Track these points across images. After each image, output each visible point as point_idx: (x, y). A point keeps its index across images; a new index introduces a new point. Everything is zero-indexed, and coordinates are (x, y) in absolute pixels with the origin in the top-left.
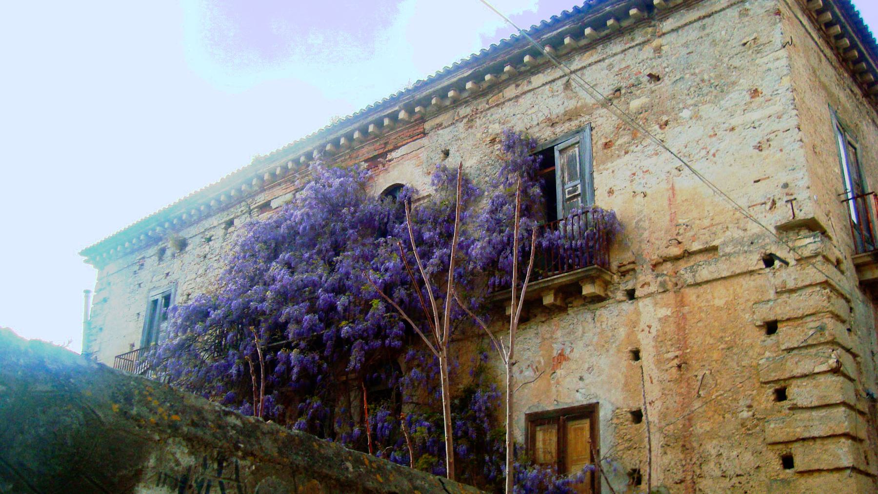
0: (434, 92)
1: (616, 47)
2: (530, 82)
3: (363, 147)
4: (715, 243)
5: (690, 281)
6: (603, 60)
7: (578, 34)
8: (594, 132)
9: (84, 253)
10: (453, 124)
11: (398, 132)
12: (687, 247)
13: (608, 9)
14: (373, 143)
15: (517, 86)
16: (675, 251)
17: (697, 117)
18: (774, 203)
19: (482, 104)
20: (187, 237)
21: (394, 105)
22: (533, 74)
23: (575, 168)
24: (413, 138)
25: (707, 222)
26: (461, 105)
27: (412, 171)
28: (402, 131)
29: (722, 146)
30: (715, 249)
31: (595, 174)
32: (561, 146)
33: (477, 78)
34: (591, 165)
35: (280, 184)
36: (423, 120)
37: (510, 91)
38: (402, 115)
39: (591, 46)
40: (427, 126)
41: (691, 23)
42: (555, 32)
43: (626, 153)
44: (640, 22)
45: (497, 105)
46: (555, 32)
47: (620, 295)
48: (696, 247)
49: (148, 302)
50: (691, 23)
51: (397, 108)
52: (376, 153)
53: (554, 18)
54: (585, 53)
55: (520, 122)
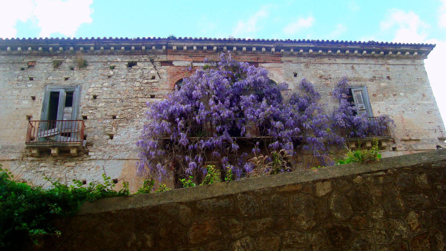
0: (294, 47)
1: (371, 61)
2: (335, 60)
3: (243, 55)
4: (420, 138)
5: (415, 149)
6: (367, 64)
7: (361, 51)
8: (368, 89)
9: (434, 46)
10: (297, 63)
11: (267, 56)
12: (411, 138)
13: (374, 48)
14: (250, 56)
15: (330, 60)
16: (407, 138)
17: (405, 96)
18: (435, 130)
19: (313, 60)
20: (88, 60)
21: (271, 44)
22: (337, 57)
23: (361, 99)
24: (275, 61)
25: (416, 131)
26: (301, 57)
27: (280, 74)
28: (269, 56)
29: (417, 108)
30: (419, 140)
31: (371, 104)
32: (355, 90)
33: (315, 49)
34: (369, 101)
35: (180, 55)
36: (281, 56)
37: (326, 60)
38: (273, 50)
39: (362, 57)
40: (283, 59)
41: (399, 65)
42: (353, 47)
43: (382, 100)
44: (382, 57)
45: (320, 64)
46: (353, 47)
47: (391, 149)
48: (413, 138)
49: (46, 92)
50: (399, 65)
51: (272, 46)
52: (253, 61)
53: (304, 40)
54: (359, 58)
55: (333, 74)
